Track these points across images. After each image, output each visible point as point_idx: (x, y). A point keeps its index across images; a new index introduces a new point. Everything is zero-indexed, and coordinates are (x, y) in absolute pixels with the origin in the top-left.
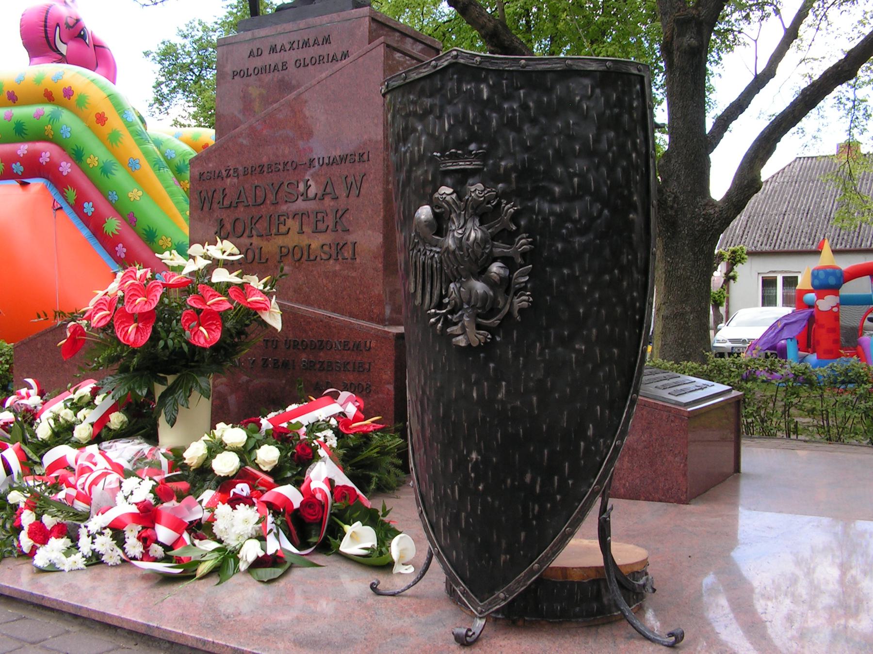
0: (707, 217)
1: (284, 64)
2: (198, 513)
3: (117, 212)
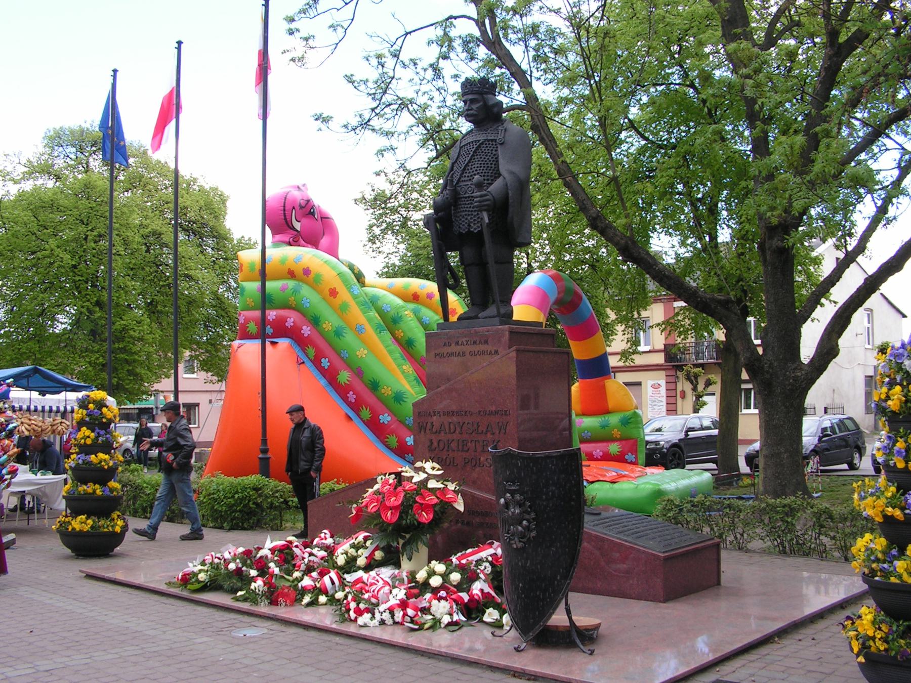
0: (796, 379)
1: (464, 353)
2: (425, 604)
3: (348, 366)
